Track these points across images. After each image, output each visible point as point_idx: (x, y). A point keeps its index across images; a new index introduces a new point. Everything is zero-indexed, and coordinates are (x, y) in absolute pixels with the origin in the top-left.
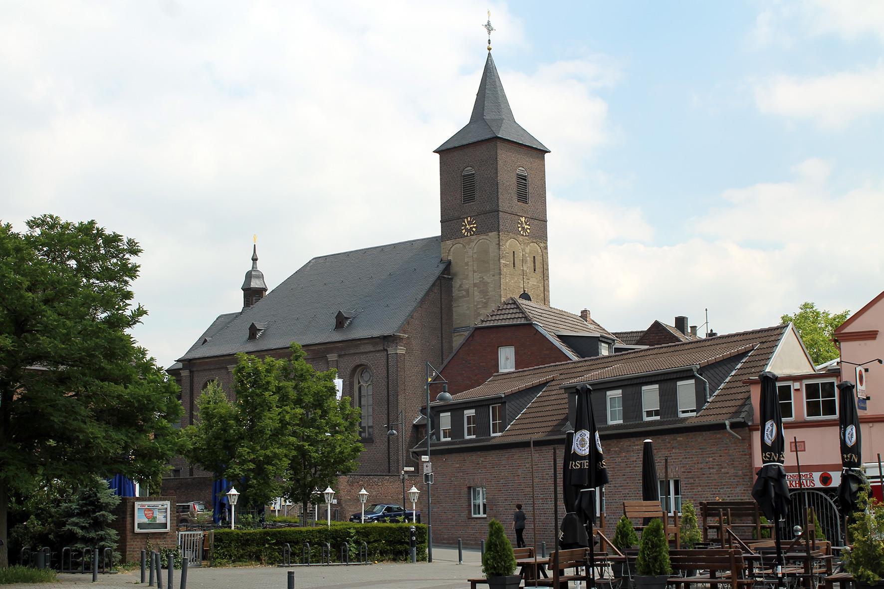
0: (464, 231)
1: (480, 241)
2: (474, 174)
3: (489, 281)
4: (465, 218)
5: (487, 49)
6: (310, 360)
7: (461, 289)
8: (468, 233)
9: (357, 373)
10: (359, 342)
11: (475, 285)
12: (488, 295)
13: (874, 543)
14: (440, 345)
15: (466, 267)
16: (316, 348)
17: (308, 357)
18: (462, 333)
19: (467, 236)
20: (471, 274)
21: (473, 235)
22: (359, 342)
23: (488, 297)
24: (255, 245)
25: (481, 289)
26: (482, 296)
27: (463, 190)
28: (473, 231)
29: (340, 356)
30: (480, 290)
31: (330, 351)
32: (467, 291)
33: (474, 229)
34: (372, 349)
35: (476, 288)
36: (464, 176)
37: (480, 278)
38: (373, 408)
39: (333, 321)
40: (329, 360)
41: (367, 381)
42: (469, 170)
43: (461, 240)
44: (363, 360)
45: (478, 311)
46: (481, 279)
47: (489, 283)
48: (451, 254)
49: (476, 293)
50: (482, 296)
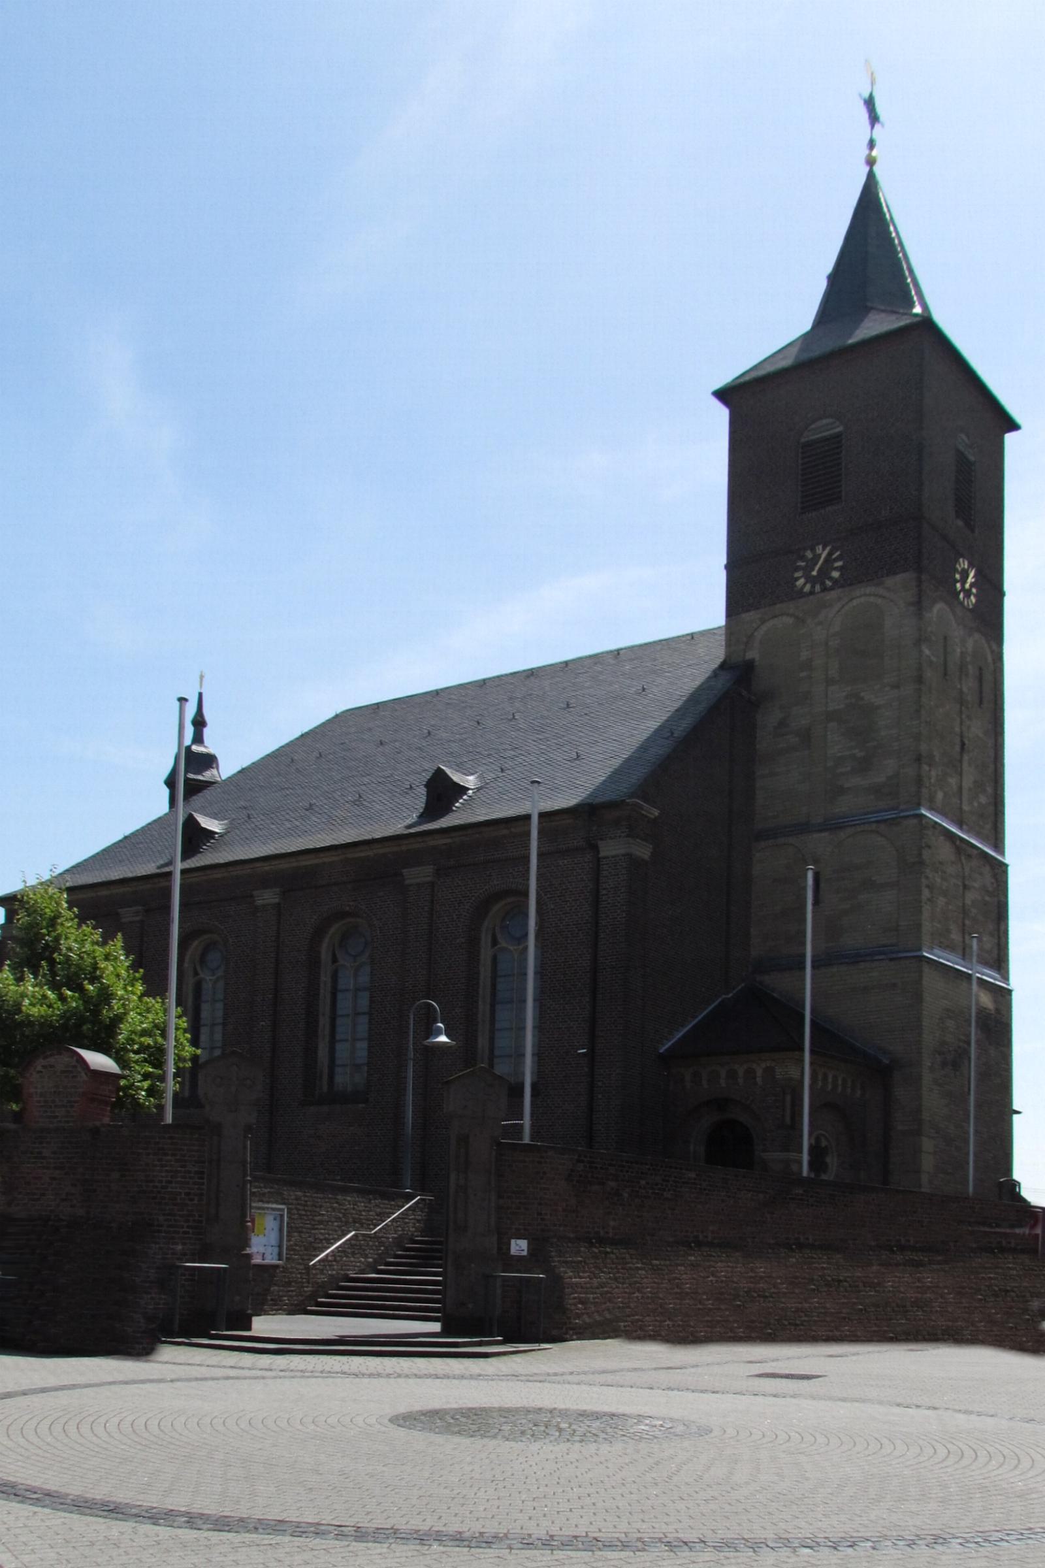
0: (801, 581)
1: (855, 602)
8: (813, 587)
10: (505, 832)
15: (803, 674)
19: (812, 593)
21: (832, 589)
22: (505, 832)
24: (200, 695)
28: (831, 578)
33: (835, 574)
39: (419, 800)
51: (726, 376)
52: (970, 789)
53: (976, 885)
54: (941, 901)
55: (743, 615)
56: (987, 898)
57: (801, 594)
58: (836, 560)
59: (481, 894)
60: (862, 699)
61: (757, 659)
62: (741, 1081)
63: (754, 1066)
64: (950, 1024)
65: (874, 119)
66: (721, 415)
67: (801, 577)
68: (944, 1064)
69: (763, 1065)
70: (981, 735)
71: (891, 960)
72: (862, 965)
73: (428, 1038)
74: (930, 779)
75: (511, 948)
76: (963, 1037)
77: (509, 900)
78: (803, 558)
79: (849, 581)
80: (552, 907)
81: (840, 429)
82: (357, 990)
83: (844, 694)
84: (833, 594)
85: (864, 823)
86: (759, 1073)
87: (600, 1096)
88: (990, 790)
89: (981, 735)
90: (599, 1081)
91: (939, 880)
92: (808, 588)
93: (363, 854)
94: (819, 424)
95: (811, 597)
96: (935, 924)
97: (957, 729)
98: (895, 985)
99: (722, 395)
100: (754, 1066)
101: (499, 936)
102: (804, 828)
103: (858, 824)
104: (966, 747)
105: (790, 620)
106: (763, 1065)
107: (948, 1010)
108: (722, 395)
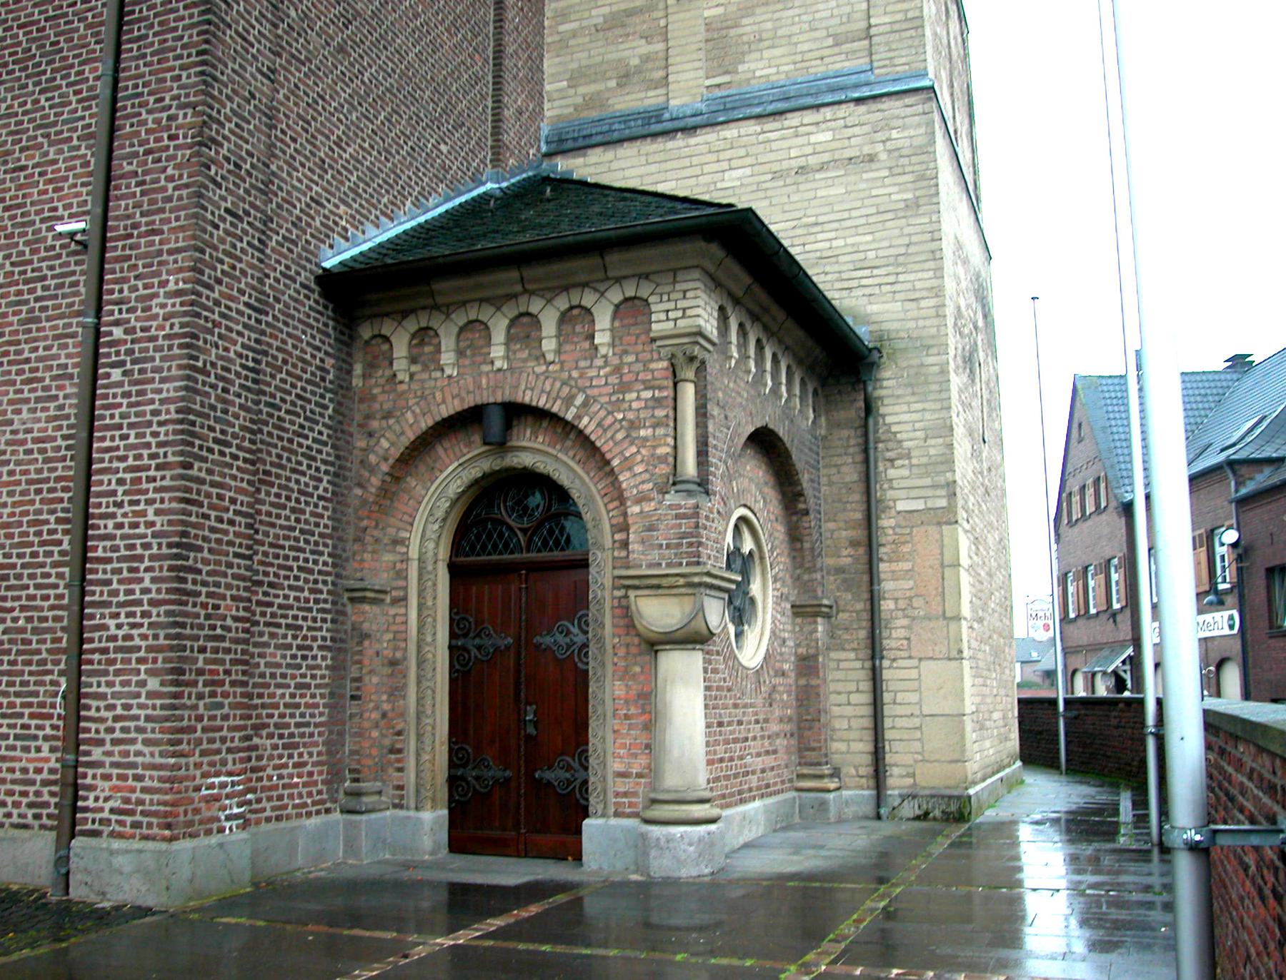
87: (116, 374)
90: (117, 323)
98: (871, 158)
106: (615, 295)
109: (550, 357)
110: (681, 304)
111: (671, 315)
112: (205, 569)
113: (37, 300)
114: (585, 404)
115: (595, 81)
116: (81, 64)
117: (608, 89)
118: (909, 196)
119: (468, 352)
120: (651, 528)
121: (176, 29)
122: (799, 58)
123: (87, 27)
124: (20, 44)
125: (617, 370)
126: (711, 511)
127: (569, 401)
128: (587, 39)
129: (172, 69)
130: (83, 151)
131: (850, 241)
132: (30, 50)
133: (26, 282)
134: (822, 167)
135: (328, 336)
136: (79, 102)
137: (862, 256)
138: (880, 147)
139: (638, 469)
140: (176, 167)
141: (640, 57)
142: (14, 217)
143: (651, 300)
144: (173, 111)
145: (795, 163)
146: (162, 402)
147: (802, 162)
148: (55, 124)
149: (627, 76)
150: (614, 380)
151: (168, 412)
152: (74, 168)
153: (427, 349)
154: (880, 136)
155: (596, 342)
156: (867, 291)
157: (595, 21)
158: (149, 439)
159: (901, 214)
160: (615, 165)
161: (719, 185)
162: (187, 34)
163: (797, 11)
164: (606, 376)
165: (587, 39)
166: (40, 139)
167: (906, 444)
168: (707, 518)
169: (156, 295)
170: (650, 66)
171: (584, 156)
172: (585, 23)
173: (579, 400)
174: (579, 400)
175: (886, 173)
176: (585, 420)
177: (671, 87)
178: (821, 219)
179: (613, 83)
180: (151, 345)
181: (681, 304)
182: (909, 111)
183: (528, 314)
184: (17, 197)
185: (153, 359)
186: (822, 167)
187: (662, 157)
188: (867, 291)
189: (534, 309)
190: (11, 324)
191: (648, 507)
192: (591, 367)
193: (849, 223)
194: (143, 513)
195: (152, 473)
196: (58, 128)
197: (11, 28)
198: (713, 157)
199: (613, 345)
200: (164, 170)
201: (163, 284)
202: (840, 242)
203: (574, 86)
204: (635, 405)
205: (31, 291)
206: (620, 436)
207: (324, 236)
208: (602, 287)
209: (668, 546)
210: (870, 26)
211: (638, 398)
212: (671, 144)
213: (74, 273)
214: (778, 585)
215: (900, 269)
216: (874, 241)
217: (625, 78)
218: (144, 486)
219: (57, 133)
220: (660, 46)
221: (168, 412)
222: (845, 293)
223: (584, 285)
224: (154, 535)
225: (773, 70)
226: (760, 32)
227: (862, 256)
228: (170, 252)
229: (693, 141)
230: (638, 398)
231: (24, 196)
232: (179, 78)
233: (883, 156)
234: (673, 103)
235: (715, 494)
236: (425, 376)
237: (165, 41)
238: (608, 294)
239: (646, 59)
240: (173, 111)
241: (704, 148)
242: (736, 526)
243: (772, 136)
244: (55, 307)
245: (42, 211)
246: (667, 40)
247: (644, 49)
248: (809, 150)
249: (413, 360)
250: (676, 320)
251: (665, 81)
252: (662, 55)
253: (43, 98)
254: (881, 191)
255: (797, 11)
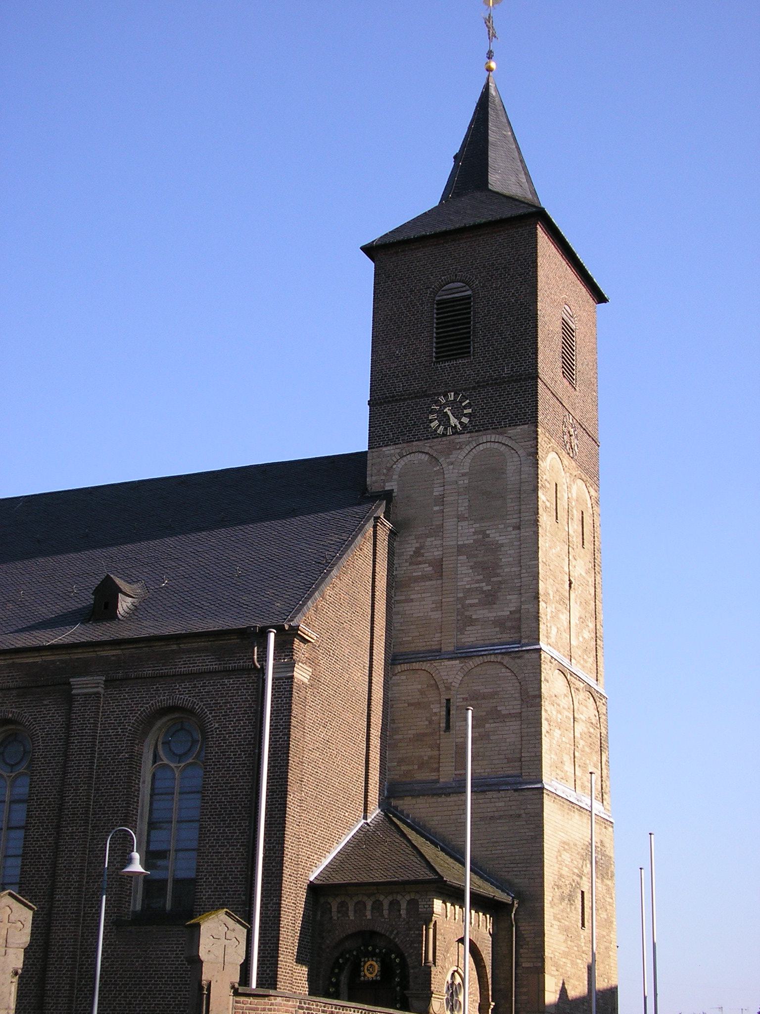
1: (481, 447)
2: (469, 297)
3: (502, 540)
4: (439, 394)
5: (485, 70)
6: (14, 692)
7: (419, 559)
9: (154, 729)
10: (174, 647)
11: (461, 550)
12: (498, 575)
13: (130, 919)
14: (493, 656)
15: (436, 508)
16: (38, 660)
17: (11, 685)
18: (416, 666)
19: (444, 435)
20: (449, 524)
22: (174, 647)
23: (500, 579)
25: (479, 559)
26: (481, 577)
27: (437, 333)
29: (109, 683)
30: (475, 563)
31: (84, 668)
32: (438, 565)
34: (214, 666)
35: (463, 558)
36: (440, 303)
37: (475, 533)
38: (201, 828)
40: (74, 692)
41: (180, 756)
42: (457, 290)
43: (426, 446)
44: (183, 695)
45: (467, 613)
46: (480, 536)
47: (502, 545)
48: (395, 477)
49: (464, 570)
50: (481, 577)
51: (374, 234)
52: (576, 625)
53: (583, 718)
54: (557, 733)
55: (384, 449)
56: (592, 730)
57: (434, 435)
58: (465, 407)
59: (147, 708)
60: (488, 536)
61: (395, 488)
62: (386, 912)
63: (399, 897)
64: (566, 856)
65: (492, 36)
66: (368, 266)
67: (439, 426)
68: (562, 899)
69: (408, 898)
70: (584, 574)
71: (516, 790)
72: (490, 795)
73: (125, 866)
74: (546, 615)
75: (172, 765)
76: (576, 871)
77: (177, 715)
78: (437, 402)
79: (477, 427)
80: (217, 726)
81: (469, 293)
82: (13, 802)
83: (473, 530)
84: (464, 438)
85: (491, 654)
86: (404, 905)
88: (592, 626)
89: (584, 574)
91: (554, 713)
92: (441, 429)
93: (31, 660)
94: (451, 285)
95: (444, 439)
96: (552, 756)
97: (567, 570)
98: (519, 816)
99: (369, 250)
100: (399, 897)
101: (161, 752)
102: (436, 654)
103: (485, 655)
104: (572, 585)
105: (425, 458)
107: (564, 843)
108: (369, 250)
109: (386, 916)
110: (428, 903)
111: (428, 906)
112: (283, 988)
113: (226, 898)
114: (397, 933)
115: (408, 764)
116: (240, 820)
117: (414, 769)
118: (533, 834)
119: (358, 912)
120: (416, 977)
121: (275, 817)
122: (493, 766)
123: (242, 807)
124: (217, 809)
125: (408, 923)
126: (437, 972)
127: (391, 932)
128: (406, 744)
129: (274, 831)
130: (241, 850)
131: (509, 851)
132: (221, 811)
133: (222, 891)
134: (500, 817)
135: (310, 904)
136: (240, 833)
137: (513, 858)
138: (522, 812)
139: (414, 957)
140: (276, 863)
141: (428, 756)
142: (217, 869)
143: (420, 900)
144: (274, 844)
145: (490, 815)
146: (272, 937)
147: (492, 814)
148: (231, 839)
149: (423, 763)
150: (406, 926)
151: (274, 940)
152: (239, 855)
153: (344, 909)
154: (523, 807)
155: (401, 912)
156: (515, 873)
157: (409, 736)
158: (267, 948)
159: (529, 841)
160: (416, 806)
161: (459, 821)
162: (278, 820)
163: (493, 745)
164: (404, 925)
165: (406, 744)
166: (226, 844)
167: (527, 939)
168: (435, 975)
169: (269, 903)
170: (432, 761)
171: (403, 800)
172: (405, 737)
173: (395, 932)
174: (395, 932)
175: (524, 823)
176: (397, 940)
177: (441, 773)
178: (498, 840)
179: (416, 767)
180: (268, 919)
181: (428, 903)
182: (535, 797)
183: (378, 900)
184: (218, 862)
185: (269, 923)
186: (500, 817)
187: (435, 805)
188: (515, 873)
189: (381, 899)
190: (217, 905)
191: (416, 970)
192: (399, 921)
193: (509, 843)
194: (266, 971)
195: (269, 959)
196: (232, 841)
197: (214, 802)
198: (456, 808)
199: (407, 914)
200: (272, 863)
201: (272, 900)
202: (506, 851)
203: (400, 766)
204: (413, 935)
205: (224, 895)
206: (408, 946)
207: (310, 870)
208: (404, 894)
209: (422, 984)
210: (522, 757)
211: (414, 933)
212: (439, 800)
213: (239, 891)
214: (472, 996)
215: (528, 865)
216: (519, 851)
217: (422, 765)
218: (266, 962)
219: (232, 842)
220: (436, 753)
221: (274, 940)
222: (506, 873)
223: (398, 893)
224: (270, 977)
225: (483, 771)
226: (478, 753)
227: (513, 858)
228: (274, 890)
229: (449, 799)
230: (414, 933)
231: (221, 862)
232: (276, 834)
233: (524, 815)
234: (441, 780)
235: (438, 966)
236: (342, 918)
237: (271, 821)
238: (405, 897)
239: (430, 758)
240: (274, 844)
241: (453, 804)
242: (453, 974)
243: (481, 801)
244: (233, 901)
245: (227, 868)
246: (439, 750)
247: (430, 753)
248: (495, 809)
249: (339, 912)
250: (427, 908)
251: (438, 770)
252: (437, 756)
253: (227, 829)
254: (522, 831)
255: (493, 745)
